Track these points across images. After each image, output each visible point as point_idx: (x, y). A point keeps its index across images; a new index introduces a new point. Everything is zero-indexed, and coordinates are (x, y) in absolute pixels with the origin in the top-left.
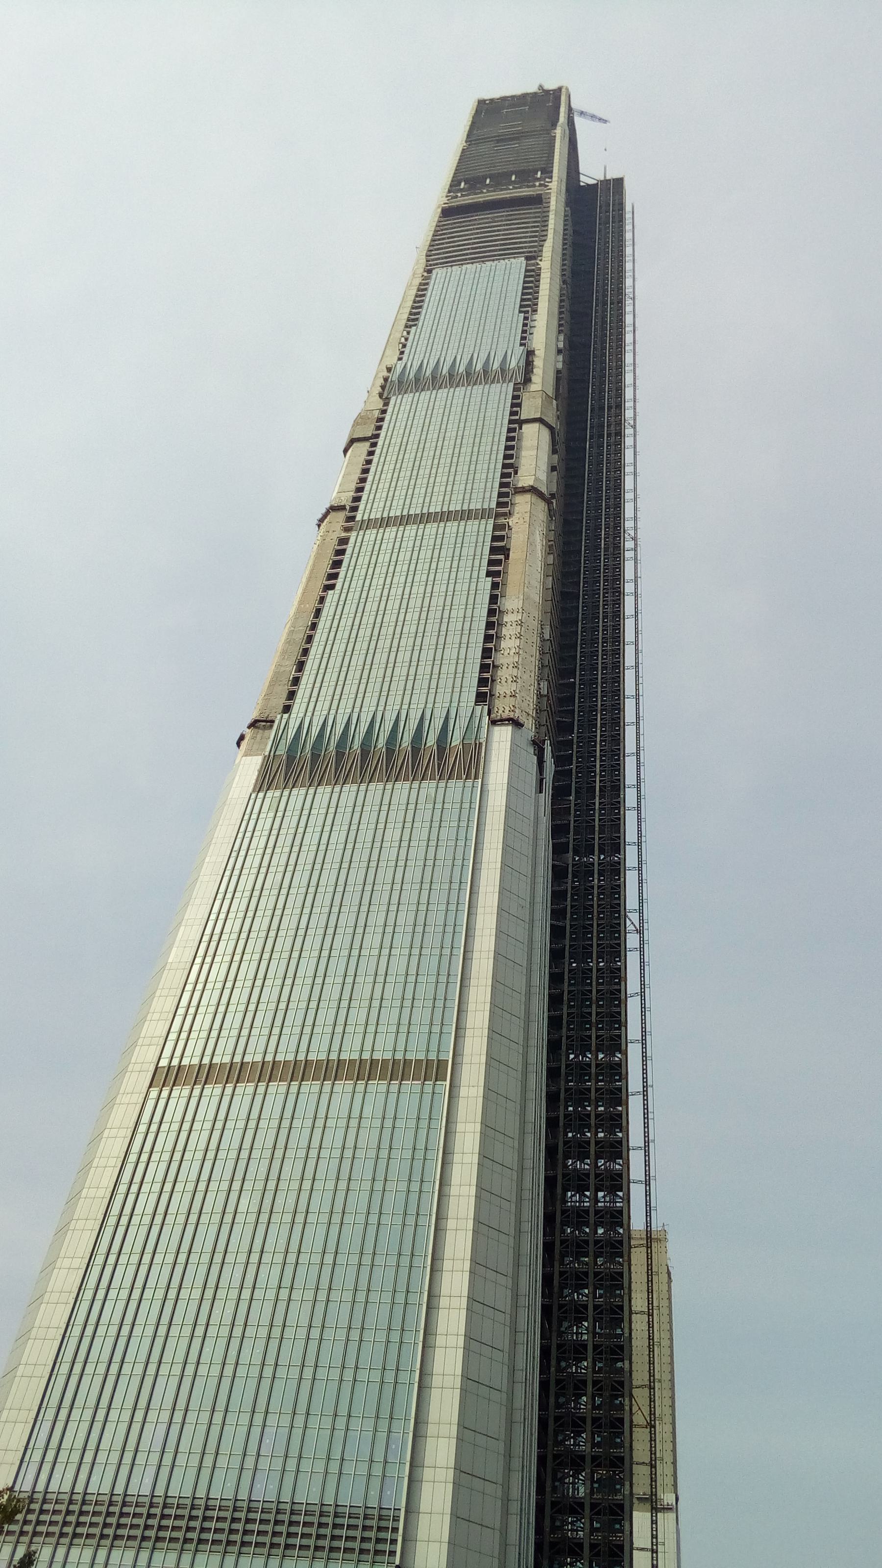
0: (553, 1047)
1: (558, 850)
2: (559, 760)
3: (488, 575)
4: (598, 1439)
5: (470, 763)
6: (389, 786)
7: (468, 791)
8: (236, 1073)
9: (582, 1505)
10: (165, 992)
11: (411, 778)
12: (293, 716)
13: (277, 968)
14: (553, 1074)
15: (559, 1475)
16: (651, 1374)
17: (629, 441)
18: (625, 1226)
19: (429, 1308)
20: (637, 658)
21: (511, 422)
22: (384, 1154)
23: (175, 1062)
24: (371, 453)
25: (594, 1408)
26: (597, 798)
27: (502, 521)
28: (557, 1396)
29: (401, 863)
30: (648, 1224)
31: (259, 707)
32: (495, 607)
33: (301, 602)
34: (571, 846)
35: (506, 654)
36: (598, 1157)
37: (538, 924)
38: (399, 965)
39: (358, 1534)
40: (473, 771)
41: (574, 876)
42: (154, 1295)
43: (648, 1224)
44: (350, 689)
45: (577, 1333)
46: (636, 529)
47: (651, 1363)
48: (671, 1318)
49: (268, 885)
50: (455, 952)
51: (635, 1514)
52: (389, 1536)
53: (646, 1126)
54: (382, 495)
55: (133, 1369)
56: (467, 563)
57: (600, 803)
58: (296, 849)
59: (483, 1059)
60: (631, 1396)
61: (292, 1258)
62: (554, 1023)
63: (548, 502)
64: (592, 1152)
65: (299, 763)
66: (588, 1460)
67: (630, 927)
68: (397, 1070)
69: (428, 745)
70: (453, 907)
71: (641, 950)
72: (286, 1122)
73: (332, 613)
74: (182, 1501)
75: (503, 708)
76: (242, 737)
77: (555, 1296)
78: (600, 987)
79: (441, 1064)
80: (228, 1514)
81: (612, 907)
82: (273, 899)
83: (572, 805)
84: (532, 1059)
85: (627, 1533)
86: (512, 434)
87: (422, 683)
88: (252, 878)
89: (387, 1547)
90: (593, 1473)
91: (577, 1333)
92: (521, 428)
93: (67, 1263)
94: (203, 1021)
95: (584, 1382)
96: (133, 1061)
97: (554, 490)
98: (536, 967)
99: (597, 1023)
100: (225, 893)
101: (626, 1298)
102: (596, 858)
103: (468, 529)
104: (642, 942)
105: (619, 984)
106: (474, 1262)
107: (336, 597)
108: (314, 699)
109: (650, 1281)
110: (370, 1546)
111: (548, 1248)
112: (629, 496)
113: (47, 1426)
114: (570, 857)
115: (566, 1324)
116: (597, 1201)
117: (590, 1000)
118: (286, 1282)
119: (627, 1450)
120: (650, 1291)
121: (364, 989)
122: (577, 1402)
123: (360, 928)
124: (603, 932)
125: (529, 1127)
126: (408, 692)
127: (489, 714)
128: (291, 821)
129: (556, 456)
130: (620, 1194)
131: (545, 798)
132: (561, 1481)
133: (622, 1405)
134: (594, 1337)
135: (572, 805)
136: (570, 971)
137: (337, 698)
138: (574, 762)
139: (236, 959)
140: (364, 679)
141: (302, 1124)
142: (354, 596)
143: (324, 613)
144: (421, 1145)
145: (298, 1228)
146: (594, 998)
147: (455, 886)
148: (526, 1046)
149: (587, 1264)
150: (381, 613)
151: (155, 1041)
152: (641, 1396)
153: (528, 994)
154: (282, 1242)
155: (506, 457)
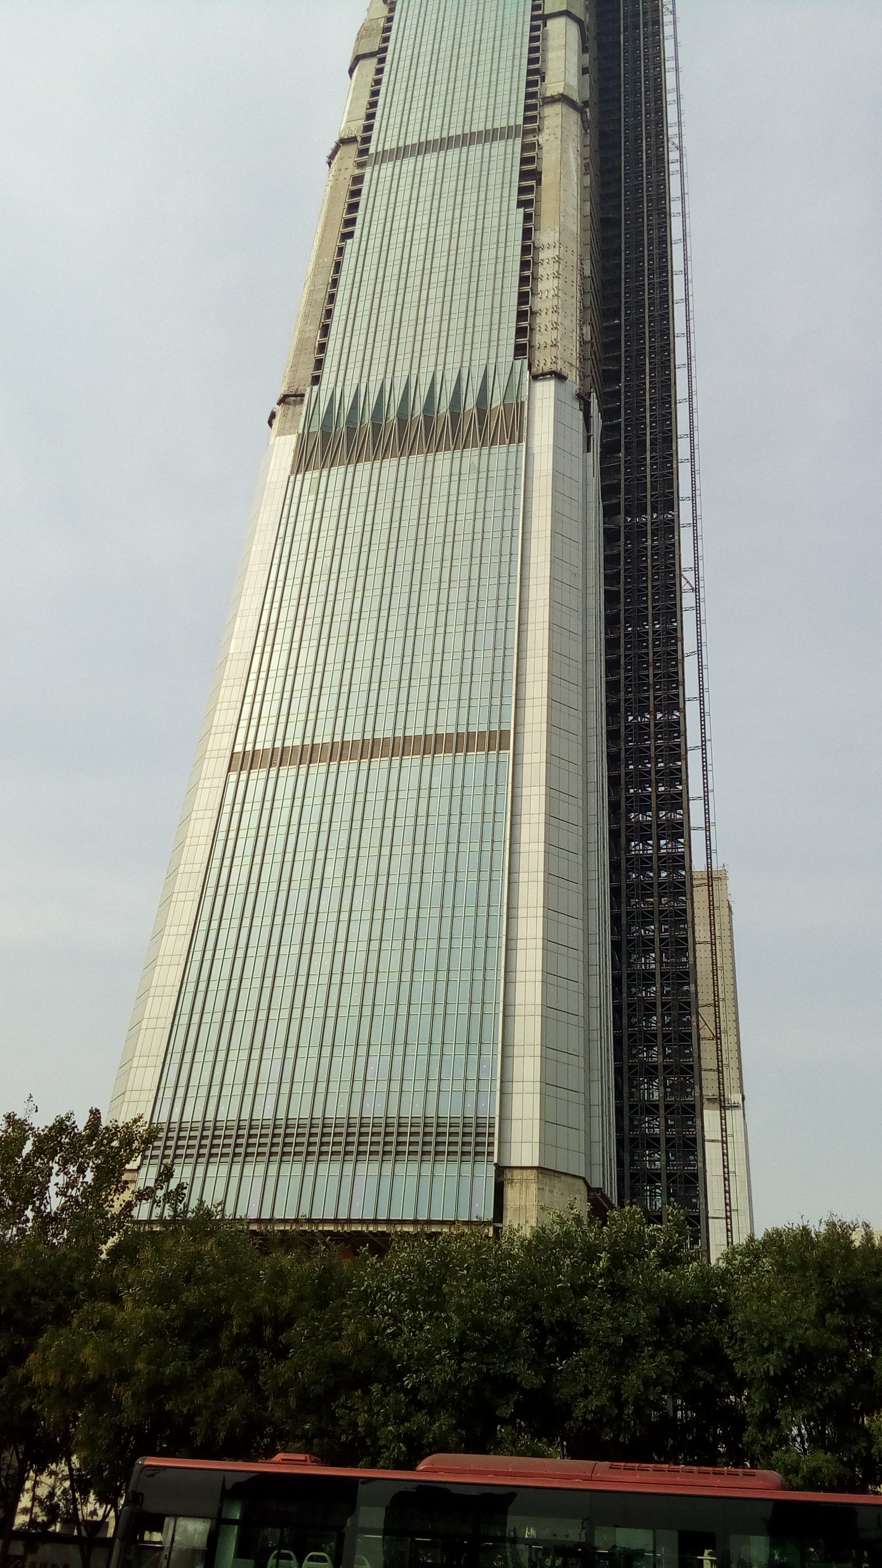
0: (612, 710)
1: (609, 512)
2: (606, 414)
3: (519, 206)
4: (668, 1051)
5: (513, 426)
6: (430, 457)
7: (512, 456)
8: (308, 754)
9: (657, 1107)
10: (230, 683)
11: (452, 447)
12: (323, 387)
13: (336, 653)
14: (612, 736)
15: (635, 1083)
16: (716, 994)
17: (668, 30)
18: (687, 869)
19: (502, 1093)
20: (687, 290)
21: (533, 18)
22: (455, 819)
23: (249, 748)
24: (380, 71)
25: (664, 1025)
26: (648, 453)
27: (530, 139)
28: (629, 1017)
29: (449, 539)
30: (709, 865)
31: (286, 380)
32: (529, 243)
33: (318, 256)
34: (622, 507)
35: (544, 297)
36: (659, 809)
37: (591, 591)
38: (455, 642)
39: (459, 1139)
40: (517, 433)
41: (626, 538)
42: (257, 953)
43: (709, 865)
44: (380, 353)
45: (645, 964)
46: (680, 136)
47: (715, 985)
48: (732, 946)
49: (317, 571)
50: (509, 625)
51: (706, 1112)
52: (486, 1139)
53: (705, 777)
54: (395, 121)
55: (247, 1016)
56: (494, 193)
57: (651, 458)
58: (341, 532)
59: (544, 727)
60: (698, 1014)
61: (378, 915)
62: (612, 687)
63: (582, 113)
64: (654, 805)
65: (336, 439)
66: (661, 1069)
67: (685, 587)
68: (461, 743)
69: (467, 409)
70: (505, 580)
71: (698, 608)
72: (360, 797)
73: (344, 312)
74: (301, 1122)
75: (544, 360)
76: (273, 416)
77: (624, 933)
78: (658, 649)
79: (504, 734)
80: (343, 1130)
81: (666, 567)
82: (324, 585)
83: (622, 463)
84: (592, 723)
85: (699, 1128)
86: (536, 34)
87: (456, 340)
88: (301, 564)
89: (486, 1149)
90: (665, 1080)
91: (645, 964)
92: (545, 25)
93: (174, 930)
94: (270, 708)
95: (654, 1005)
96: (209, 748)
97: (587, 96)
98: (591, 634)
99: (655, 684)
100: (274, 585)
101: (689, 902)
102: (649, 517)
103: (494, 152)
104: (698, 600)
105: (676, 644)
106: (545, 1046)
107: (356, 246)
108: (343, 367)
109: (712, 915)
110: (470, 1149)
111: (615, 892)
112: (671, 97)
113: (174, 1068)
114: (622, 519)
115: (635, 956)
116: (659, 848)
117: (647, 662)
118: (376, 935)
119: (696, 1059)
120: (712, 924)
121: (422, 669)
122: (647, 1021)
123: (413, 609)
124: (657, 594)
125: (592, 787)
126: (442, 351)
127: (530, 368)
128: (332, 503)
129: (587, 56)
130: (682, 840)
131: (594, 458)
132: (637, 1087)
133: (689, 1021)
134: (661, 965)
135: (622, 463)
136: (626, 635)
137: (367, 363)
138: (623, 413)
139: (295, 646)
140: (394, 341)
141: (375, 799)
142: (374, 243)
143: (344, 267)
144: (490, 809)
145: (381, 890)
146: (651, 660)
147: (506, 558)
148: (585, 712)
149: (652, 904)
150: (410, 229)
151: (228, 728)
152: (707, 1014)
153: (586, 661)
154: (369, 901)
155: (531, 61)
